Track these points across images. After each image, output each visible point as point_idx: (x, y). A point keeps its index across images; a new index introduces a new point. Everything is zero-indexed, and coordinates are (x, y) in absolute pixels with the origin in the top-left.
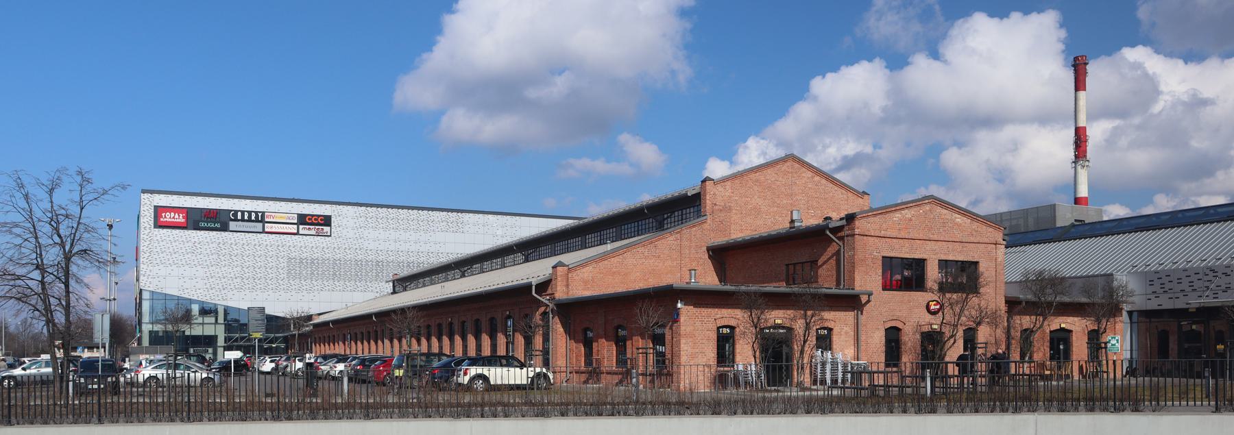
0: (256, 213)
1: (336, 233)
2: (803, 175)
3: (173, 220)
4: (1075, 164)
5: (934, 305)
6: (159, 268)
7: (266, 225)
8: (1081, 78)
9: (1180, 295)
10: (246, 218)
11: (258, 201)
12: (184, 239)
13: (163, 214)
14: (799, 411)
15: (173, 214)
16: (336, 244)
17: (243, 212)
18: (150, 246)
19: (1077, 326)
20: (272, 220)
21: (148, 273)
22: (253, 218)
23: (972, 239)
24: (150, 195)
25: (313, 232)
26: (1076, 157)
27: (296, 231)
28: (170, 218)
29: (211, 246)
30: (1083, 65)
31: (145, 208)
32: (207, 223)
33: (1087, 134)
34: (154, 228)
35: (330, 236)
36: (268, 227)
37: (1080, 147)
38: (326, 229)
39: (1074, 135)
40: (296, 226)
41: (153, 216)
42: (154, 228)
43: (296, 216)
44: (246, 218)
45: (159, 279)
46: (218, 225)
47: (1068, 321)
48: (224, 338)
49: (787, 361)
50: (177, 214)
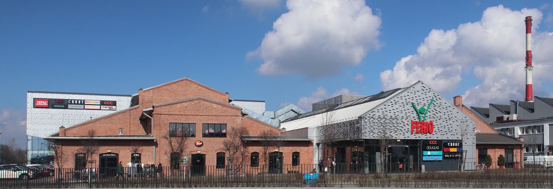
0: (81, 100)
1: (118, 109)
2: (192, 86)
3: (42, 104)
4: (526, 69)
5: (199, 143)
6: (47, 126)
7: (85, 106)
8: (529, 27)
9: (445, 133)
10: (76, 103)
11: (93, 96)
12: (47, 113)
13: (38, 102)
14: (386, 186)
15: (42, 102)
16: (92, 113)
17: (75, 100)
18: (31, 116)
19: (287, 152)
20: (88, 103)
21: (30, 128)
22: (79, 103)
23: (222, 114)
24: (31, 93)
25: (108, 109)
26: (527, 65)
27: (99, 108)
28: (41, 103)
29: (60, 115)
30: (530, 21)
31: (29, 99)
32: (58, 105)
33: (532, 54)
34: (34, 108)
35: (116, 110)
36: (86, 107)
37: (528, 60)
38: (114, 107)
39: (526, 55)
40: (99, 106)
41: (33, 103)
42: (34, 108)
43: (99, 101)
44: (76, 103)
45: (47, 131)
46: (63, 106)
48: (545, 150)
50: (44, 102)
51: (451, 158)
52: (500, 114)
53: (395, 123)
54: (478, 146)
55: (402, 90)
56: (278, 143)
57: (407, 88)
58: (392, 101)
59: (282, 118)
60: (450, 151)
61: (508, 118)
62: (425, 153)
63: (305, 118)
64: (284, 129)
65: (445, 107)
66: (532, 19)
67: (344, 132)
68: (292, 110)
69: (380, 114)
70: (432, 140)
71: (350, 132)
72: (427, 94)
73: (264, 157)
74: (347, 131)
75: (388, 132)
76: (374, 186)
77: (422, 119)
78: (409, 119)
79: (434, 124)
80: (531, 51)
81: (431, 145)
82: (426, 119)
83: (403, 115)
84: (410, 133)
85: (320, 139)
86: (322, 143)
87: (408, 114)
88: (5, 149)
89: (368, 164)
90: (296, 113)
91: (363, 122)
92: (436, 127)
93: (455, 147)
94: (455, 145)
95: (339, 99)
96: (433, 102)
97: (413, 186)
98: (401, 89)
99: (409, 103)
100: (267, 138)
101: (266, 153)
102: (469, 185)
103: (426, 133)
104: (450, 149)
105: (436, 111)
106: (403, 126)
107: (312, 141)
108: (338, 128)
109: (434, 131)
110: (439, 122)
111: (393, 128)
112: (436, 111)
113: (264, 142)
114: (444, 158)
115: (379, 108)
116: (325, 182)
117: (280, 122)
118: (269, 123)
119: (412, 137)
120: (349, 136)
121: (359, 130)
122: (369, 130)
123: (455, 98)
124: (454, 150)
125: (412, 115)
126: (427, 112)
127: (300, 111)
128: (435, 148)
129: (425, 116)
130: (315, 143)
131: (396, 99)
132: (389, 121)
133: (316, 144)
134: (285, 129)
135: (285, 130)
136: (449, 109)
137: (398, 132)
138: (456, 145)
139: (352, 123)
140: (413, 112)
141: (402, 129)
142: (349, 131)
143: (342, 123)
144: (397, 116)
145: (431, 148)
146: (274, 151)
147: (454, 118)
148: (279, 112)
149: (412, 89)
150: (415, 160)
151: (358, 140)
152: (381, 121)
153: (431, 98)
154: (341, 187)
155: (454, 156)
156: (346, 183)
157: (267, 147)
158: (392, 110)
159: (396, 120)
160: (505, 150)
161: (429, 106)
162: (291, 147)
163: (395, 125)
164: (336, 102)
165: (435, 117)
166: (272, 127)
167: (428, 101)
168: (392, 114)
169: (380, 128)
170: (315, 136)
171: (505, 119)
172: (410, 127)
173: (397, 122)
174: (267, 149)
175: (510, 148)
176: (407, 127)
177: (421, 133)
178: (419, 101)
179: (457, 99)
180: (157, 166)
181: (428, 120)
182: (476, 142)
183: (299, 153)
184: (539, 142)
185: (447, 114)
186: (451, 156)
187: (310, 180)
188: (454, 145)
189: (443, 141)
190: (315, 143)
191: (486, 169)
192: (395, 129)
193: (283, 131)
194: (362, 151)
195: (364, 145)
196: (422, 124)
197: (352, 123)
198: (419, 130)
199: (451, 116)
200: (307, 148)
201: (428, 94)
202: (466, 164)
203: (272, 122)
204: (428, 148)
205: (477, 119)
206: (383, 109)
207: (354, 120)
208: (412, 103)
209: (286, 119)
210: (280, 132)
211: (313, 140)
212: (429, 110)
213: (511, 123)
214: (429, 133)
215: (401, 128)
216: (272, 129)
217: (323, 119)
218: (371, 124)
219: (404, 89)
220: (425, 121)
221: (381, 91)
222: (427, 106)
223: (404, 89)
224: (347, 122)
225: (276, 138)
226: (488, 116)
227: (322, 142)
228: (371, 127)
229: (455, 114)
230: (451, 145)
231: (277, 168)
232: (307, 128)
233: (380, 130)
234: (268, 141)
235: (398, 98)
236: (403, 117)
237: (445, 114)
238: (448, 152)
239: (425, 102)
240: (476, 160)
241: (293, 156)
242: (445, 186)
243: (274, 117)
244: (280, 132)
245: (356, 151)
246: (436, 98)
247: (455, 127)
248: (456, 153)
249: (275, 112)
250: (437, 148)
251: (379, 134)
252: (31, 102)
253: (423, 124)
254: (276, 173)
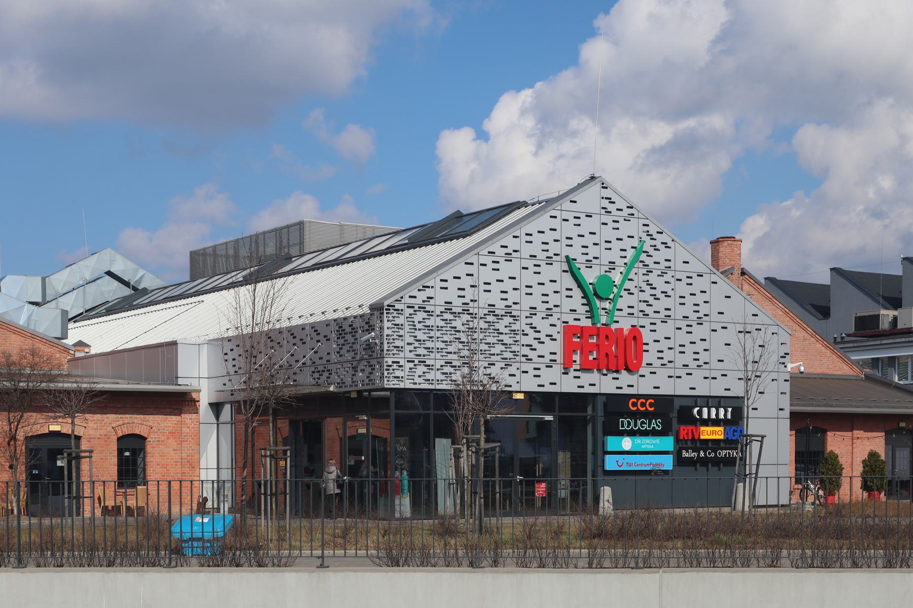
9: (682, 372)
14: (485, 563)
47: (95, 418)
49: (122, 469)
51: (704, 462)
52: (867, 307)
53: (507, 330)
54: (796, 418)
55: (530, 209)
56: (69, 399)
57: (549, 202)
58: (495, 247)
59: (73, 304)
60: (702, 437)
61: (895, 319)
62: (612, 443)
63: (162, 306)
64: (80, 344)
65: (683, 276)
67: (318, 362)
68: (109, 273)
69: (451, 295)
70: (638, 397)
71: (338, 362)
72: (622, 224)
73: (8, 454)
74: (328, 357)
75: (481, 363)
76: (441, 562)
77: (604, 320)
78: (556, 316)
79: (647, 336)
81: (635, 415)
82: (615, 319)
83: (536, 300)
84: (558, 369)
85: (224, 388)
86: (231, 403)
87: (553, 299)
88: (11, 370)
89: (406, 483)
90: (126, 284)
91: (389, 324)
92: (653, 348)
93: (716, 422)
94: (717, 415)
95: (294, 239)
96: (643, 257)
97: (583, 562)
98: (525, 204)
99: (555, 258)
100: (41, 382)
101: (13, 438)
102: (778, 558)
103: (617, 371)
104: (702, 428)
105: (653, 292)
106: (535, 344)
107: (194, 395)
108: (294, 344)
109: (644, 364)
110: (664, 330)
111: (498, 348)
112: (653, 292)
113: (8, 394)
114: (680, 461)
115: (448, 274)
116: (256, 548)
117: (68, 319)
118: (21, 323)
119: (569, 385)
120: (334, 377)
121: (375, 355)
122: (412, 355)
123: (715, 243)
124: (713, 432)
125: (567, 305)
126: (619, 292)
127: (141, 278)
128: (646, 426)
129: (615, 305)
130: (204, 400)
131: (508, 240)
132: (483, 325)
133: (210, 404)
134: (88, 346)
135: (87, 350)
136: (699, 284)
137: (518, 365)
138: (722, 416)
139: (348, 329)
140: (569, 293)
141: (532, 354)
142: (334, 357)
143: (307, 328)
144: (514, 307)
145: (636, 425)
146: (47, 432)
147: (715, 316)
148: (60, 280)
149: (567, 205)
150: (578, 469)
151: (370, 391)
152: (454, 324)
153: (635, 242)
154: (322, 566)
155: (713, 455)
156: (340, 552)
157: (17, 415)
158: (494, 282)
159: (465, 317)
160: (888, 433)
161: (628, 272)
162: (112, 417)
163: (507, 339)
164: (280, 247)
165: (648, 310)
166: (33, 336)
167: (623, 254)
168: (494, 297)
169: (450, 349)
170: (204, 373)
171: (885, 325)
172: (558, 346)
173: (514, 327)
174: (19, 422)
175: (903, 428)
176: (550, 346)
177: (599, 370)
178: (593, 251)
179: (724, 249)
180: (843, 466)
181: (625, 324)
182: (791, 405)
183: (146, 439)
185: (690, 300)
186: (702, 454)
187: (192, 539)
188: (713, 416)
189: (675, 399)
190: (204, 400)
191: (822, 500)
192: (508, 355)
193: (78, 355)
194: (385, 434)
195: (393, 411)
196: (603, 336)
197: (348, 329)
198: (591, 358)
199: (703, 309)
200: (174, 419)
201: (626, 228)
202: (761, 483)
203: (33, 318)
204: (625, 423)
205: (791, 323)
206: (463, 276)
207: (355, 317)
208: (567, 257)
209: (88, 307)
210: (65, 359)
211: (199, 391)
212: (628, 285)
213: (907, 340)
214: (628, 370)
215: (526, 351)
216: (38, 345)
217: (238, 309)
218: (417, 333)
219: (537, 206)
220: (614, 326)
221: (448, 211)
222: (622, 269)
223: (537, 206)
224: (327, 324)
225: (52, 379)
226: (824, 312)
227: (232, 399)
228: (417, 344)
229: (719, 303)
230: (705, 416)
231: (66, 496)
232: (174, 344)
233: (450, 356)
234: (24, 391)
235: (514, 237)
236: (533, 311)
237: (682, 301)
238: (693, 440)
239: (615, 255)
240: (789, 470)
241: (120, 452)
242: (695, 563)
243: (39, 300)
244: (65, 359)
245: (362, 434)
246: (653, 243)
247: (718, 351)
248: (722, 445)
249: (44, 280)
250: (656, 424)
251: (448, 369)
253: (607, 337)
254: (59, 512)
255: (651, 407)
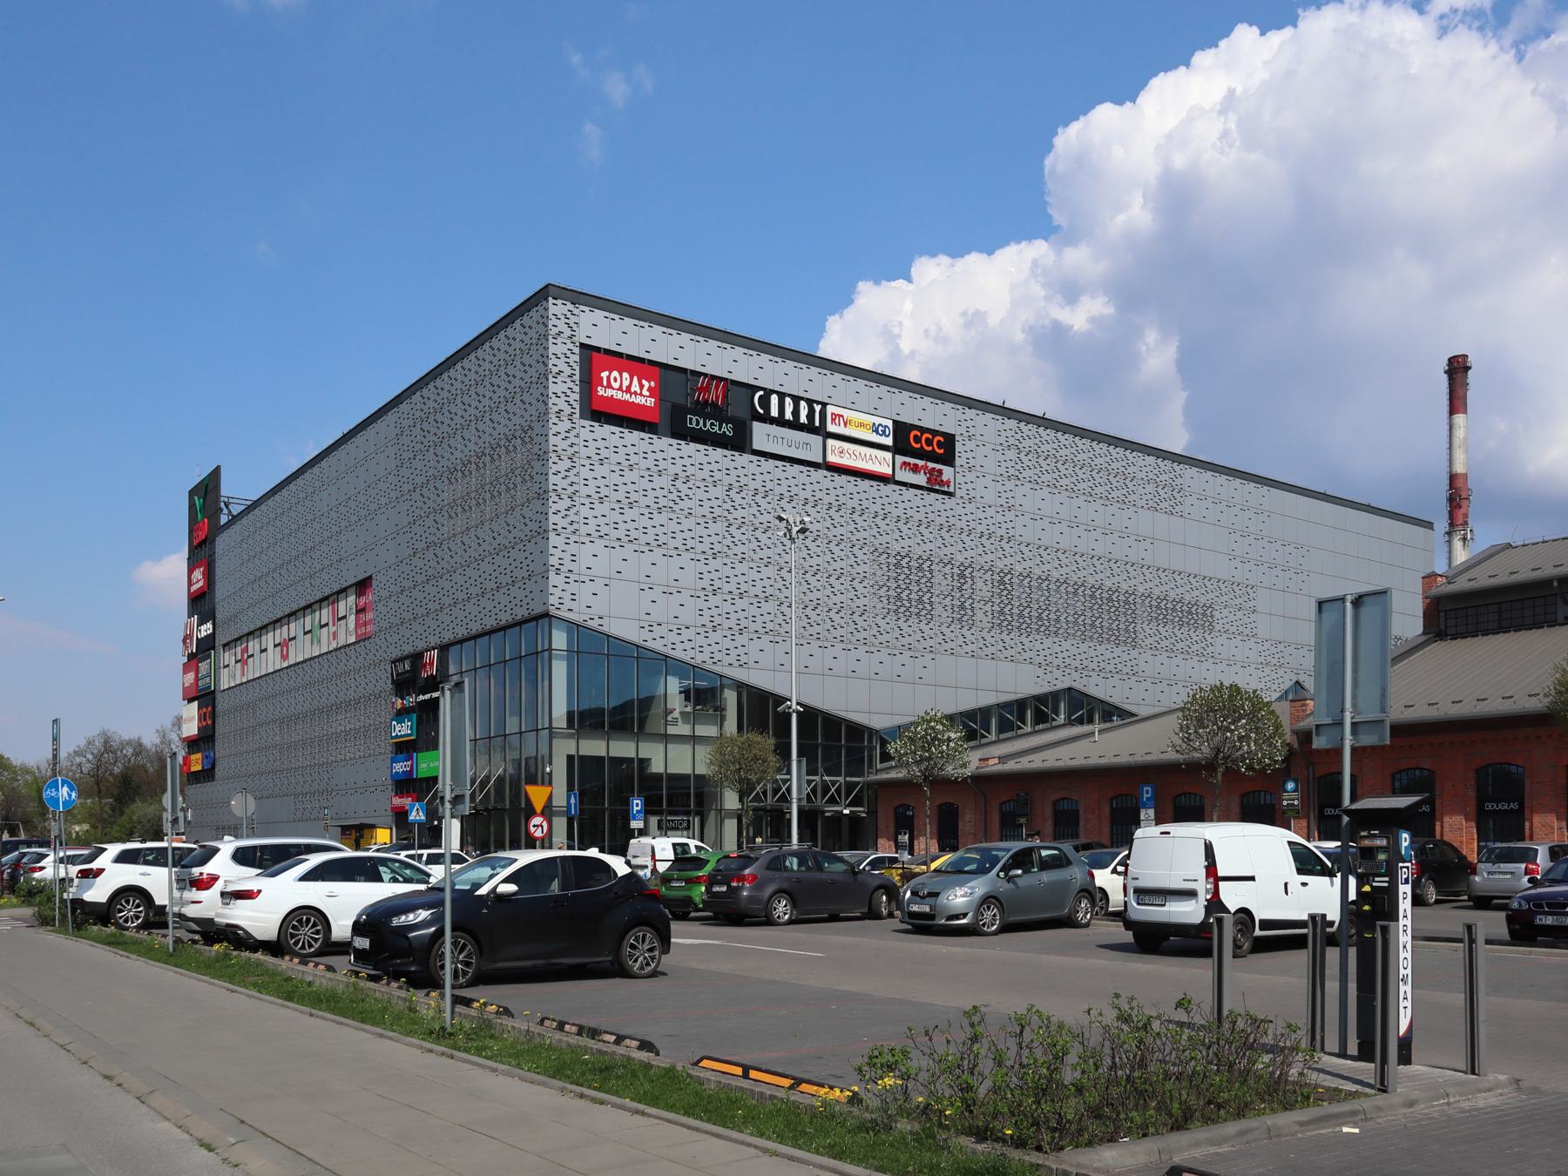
3: (626, 397)
7: (830, 442)
8: (1460, 392)
13: (604, 375)
25: (921, 479)
28: (620, 389)
66: (1469, 364)
80: (1466, 474)
128: (717, 428)
184: (1422, 910)
229: (980, 429)
237: (701, 576)
252: (568, 371)
255: (939, 448)
